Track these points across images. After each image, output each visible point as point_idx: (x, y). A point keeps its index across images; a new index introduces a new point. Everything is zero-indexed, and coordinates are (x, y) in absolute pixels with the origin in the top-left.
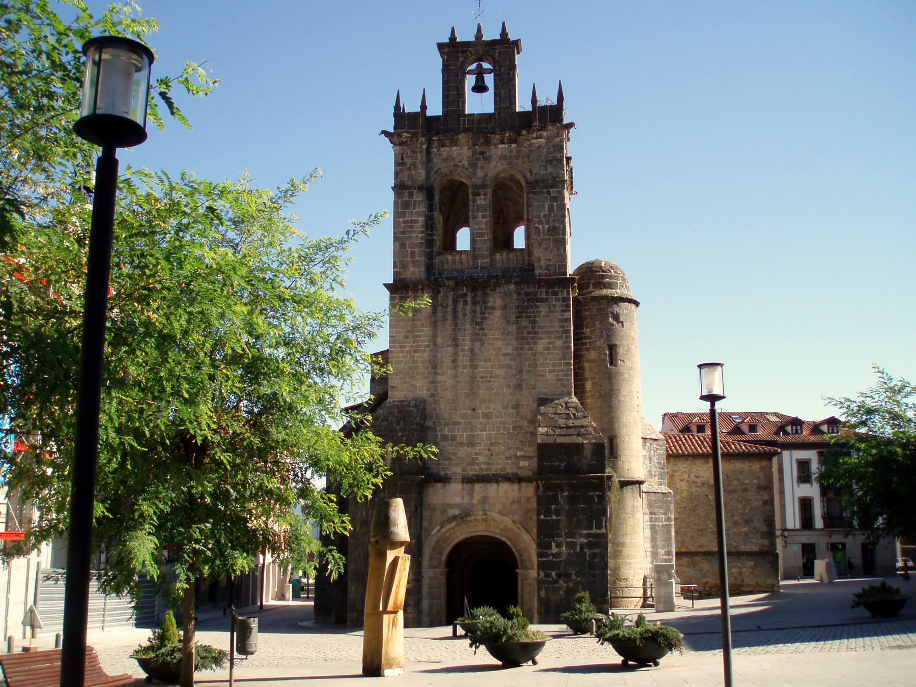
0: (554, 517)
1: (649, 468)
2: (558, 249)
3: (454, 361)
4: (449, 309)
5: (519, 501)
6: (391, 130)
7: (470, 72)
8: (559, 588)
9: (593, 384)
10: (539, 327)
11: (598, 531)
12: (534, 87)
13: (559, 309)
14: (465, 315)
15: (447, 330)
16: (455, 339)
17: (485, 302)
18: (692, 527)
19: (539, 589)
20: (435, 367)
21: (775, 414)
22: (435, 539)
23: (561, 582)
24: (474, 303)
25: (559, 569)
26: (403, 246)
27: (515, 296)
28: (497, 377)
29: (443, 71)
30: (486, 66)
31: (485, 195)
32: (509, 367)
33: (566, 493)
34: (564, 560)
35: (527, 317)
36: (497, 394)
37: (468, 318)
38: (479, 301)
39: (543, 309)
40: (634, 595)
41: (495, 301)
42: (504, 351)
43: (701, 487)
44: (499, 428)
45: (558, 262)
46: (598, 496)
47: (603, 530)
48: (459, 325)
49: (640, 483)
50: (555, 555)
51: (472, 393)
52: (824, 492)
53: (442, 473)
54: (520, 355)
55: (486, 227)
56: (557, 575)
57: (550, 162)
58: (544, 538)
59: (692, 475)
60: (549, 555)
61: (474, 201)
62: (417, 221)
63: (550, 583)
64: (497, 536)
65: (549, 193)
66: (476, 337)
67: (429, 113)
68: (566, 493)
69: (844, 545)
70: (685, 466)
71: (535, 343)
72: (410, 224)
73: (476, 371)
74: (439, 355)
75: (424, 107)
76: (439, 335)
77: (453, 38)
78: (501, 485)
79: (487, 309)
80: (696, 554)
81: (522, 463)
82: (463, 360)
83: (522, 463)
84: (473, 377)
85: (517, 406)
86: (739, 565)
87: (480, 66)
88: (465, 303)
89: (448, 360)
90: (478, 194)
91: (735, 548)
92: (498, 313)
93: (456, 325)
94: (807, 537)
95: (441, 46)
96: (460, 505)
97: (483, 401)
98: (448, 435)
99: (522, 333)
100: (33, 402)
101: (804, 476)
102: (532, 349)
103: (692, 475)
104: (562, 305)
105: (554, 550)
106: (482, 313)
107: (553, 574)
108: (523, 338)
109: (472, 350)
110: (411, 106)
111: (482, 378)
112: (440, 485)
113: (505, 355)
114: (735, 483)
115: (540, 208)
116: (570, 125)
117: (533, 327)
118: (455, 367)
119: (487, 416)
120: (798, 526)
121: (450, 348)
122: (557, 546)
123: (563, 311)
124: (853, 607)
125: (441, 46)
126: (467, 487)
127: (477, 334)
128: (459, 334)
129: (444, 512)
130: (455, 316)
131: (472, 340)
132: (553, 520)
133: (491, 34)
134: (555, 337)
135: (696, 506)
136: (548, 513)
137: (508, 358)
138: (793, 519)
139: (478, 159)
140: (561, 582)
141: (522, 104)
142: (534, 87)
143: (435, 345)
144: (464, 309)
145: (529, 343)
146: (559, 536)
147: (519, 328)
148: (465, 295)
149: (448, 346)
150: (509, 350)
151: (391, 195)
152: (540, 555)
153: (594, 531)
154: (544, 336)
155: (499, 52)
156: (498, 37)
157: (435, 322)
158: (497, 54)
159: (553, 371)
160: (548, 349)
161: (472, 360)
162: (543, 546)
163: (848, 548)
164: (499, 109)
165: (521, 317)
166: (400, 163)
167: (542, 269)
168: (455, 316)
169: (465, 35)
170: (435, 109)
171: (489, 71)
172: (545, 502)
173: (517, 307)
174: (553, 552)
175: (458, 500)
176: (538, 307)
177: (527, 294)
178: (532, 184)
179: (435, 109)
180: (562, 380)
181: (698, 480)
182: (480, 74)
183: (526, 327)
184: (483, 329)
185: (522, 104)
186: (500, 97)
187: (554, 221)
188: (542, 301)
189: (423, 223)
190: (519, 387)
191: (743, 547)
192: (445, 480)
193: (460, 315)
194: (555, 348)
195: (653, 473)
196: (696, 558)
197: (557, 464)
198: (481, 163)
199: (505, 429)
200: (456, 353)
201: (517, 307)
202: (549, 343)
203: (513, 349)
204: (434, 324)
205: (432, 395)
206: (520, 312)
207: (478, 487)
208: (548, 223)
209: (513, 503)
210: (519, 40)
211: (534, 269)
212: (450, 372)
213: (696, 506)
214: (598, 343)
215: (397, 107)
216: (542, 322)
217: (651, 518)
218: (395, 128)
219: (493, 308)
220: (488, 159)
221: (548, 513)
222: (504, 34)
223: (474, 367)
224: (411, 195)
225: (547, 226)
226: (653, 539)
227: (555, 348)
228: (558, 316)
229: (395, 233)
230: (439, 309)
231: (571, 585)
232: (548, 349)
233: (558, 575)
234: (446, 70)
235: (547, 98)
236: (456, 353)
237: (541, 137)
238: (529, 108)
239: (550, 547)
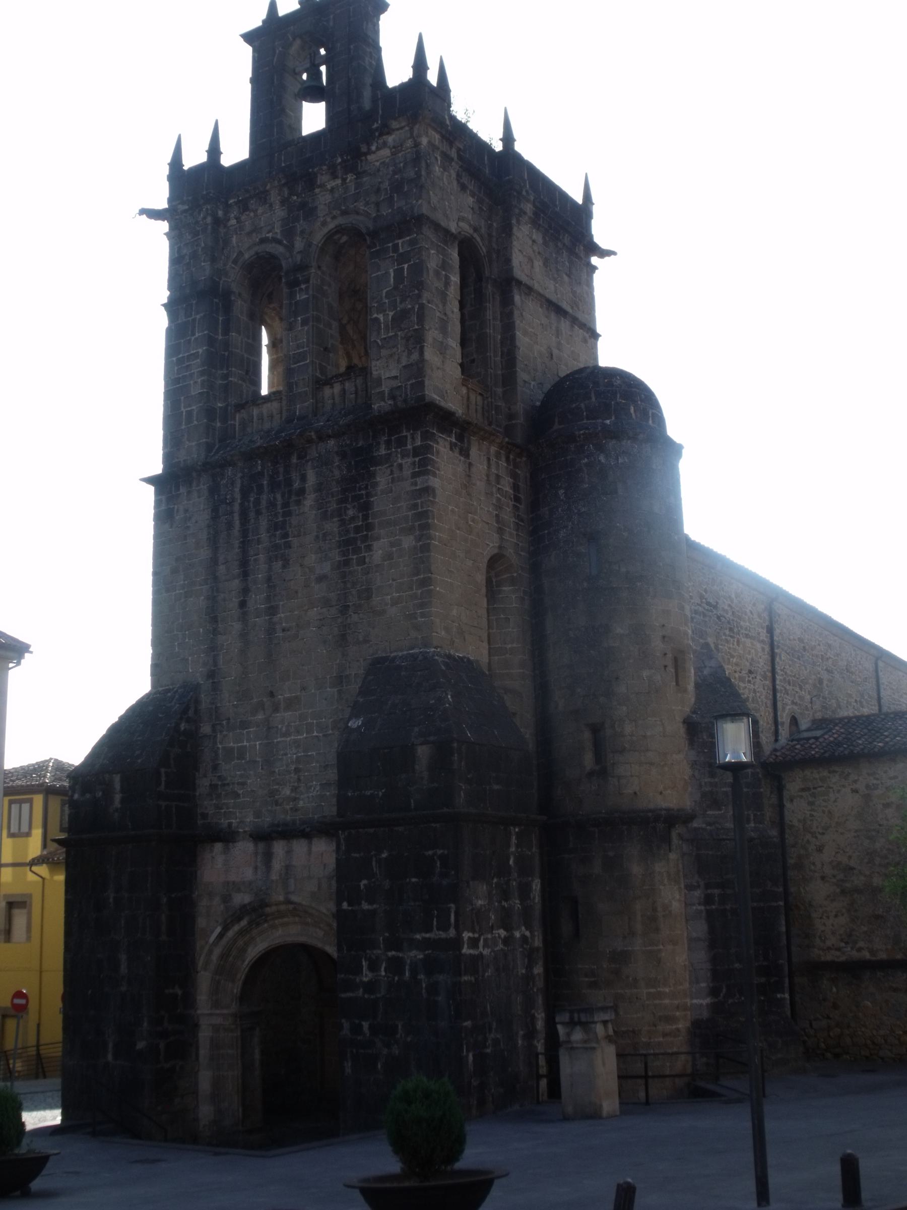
0: (365, 906)
2: (410, 354)
3: (243, 604)
4: (237, 507)
11: (443, 935)
13: (407, 472)
22: (217, 952)
41: (303, 478)
45: (408, 380)
47: (452, 933)
48: (250, 534)
53: (224, 822)
61: (292, 295)
64: (320, 945)
71: (369, 548)
75: (214, 150)
78: (315, 841)
82: (257, 600)
84: (271, 631)
98: (232, 749)
100: (825, 738)
102: (362, 561)
104: (414, 463)
105: (367, 976)
106: (286, 505)
107: (366, 1025)
111: (284, 630)
112: (218, 846)
117: (365, 517)
119: (291, 704)
126: (261, 846)
129: (226, 899)
143: (215, 578)
144: (257, 502)
147: (343, 522)
148: (261, 474)
153: (436, 934)
161: (268, 599)
167: (384, 400)
174: (365, 979)
175: (248, 874)
183: (353, 519)
192: (227, 837)
193: (252, 515)
197: (368, 793)
198: (301, 225)
200: (245, 591)
202: (392, 545)
207: (279, 848)
216: (380, 504)
219: (302, 492)
223: (272, 611)
225: (391, 314)
231: (396, 1051)
236: (245, 591)
237: (385, 144)
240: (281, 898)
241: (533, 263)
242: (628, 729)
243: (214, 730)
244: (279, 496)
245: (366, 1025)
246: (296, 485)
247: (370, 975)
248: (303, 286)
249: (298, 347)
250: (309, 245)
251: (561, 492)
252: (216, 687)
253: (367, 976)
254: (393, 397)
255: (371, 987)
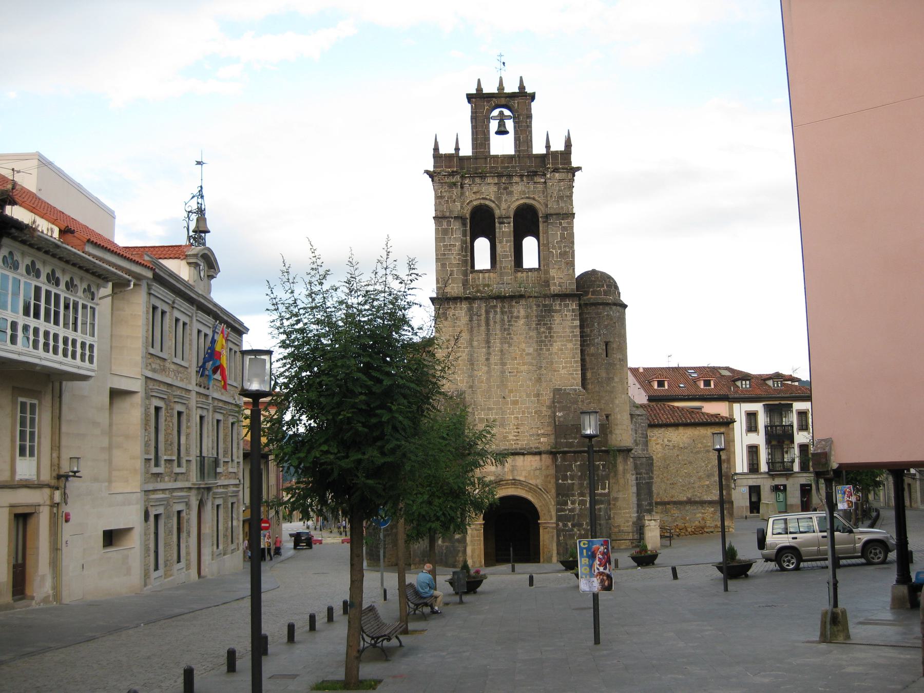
1: (635, 438)
2: (568, 270)
3: (488, 359)
5: (540, 469)
6: (431, 169)
7: (494, 118)
8: (574, 535)
9: (592, 373)
10: (554, 332)
11: (603, 491)
12: (548, 135)
14: (495, 322)
15: (482, 335)
16: (488, 342)
17: (511, 312)
18: (665, 481)
19: (558, 536)
20: (472, 364)
21: (727, 369)
23: (575, 530)
24: (503, 313)
25: (574, 520)
26: (443, 265)
27: (535, 308)
28: (522, 372)
29: (472, 118)
30: (507, 112)
31: (509, 223)
32: (531, 364)
33: (579, 463)
34: (577, 514)
35: (545, 324)
36: (522, 386)
37: (498, 327)
38: (506, 311)
39: (557, 318)
40: (621, 538)
41: (519, 312)
42: (527, 351)
43: (672, 449)
44: (523, 412)
46: (602, 465)
47: (607, 491)
48: (491, 331)
49: (630, 450)
50: (570, 510)
51: (503, 384)
52: (768, 441)
54: (539, 355)
55: (510, 250)
56: (572, 524)
57: (561, 198)
58: (562, 497)
59: (666, 440)
60: (565, 510)
61: (500, 228)
62: (454, 245)
63: (567, 531)
65: (561, 224)
66: (504, 341)
67: (461, 154)
68: (579, 463)
69: (785, 486)
70: (660, 432)
71: (551, 345)
72: (448, 247)
73: (505, 367)
74: (475, 355)
76: (475, 339)
77: (479, 89)
79: (513, 318)
80: (668, 503)
81: (542, 440)
83: (542, 440)
84: (503, 372)
85: (538, 395)
86: (703, 511)
87: (501, 113)
88: (496, 312)
89: (482, 358)
90: (503, 223)
91: (699, 497)
92: (522, 322)
93: (488, 330)
94: (753, 480)
95: (470, 97)
96: (494, 472)
97: (511, 391)
99: (541, 337)
101: (752, 427)
103: (666, 440)
105: (570, 506)
106: (509, 321)
107: (570, 524)
108: (542, 341)
109: (502, 351)
110: (447, 148)
113: (528, 354)
114: (700, 445)
115: (554, 233)
116: (579, 169)
117: (550, 333)
118: (488, 366)
119: (515, 403)
120: (746, 470)
121: (484, 350)
122: (572, 504)
123: (572, 320)
124: (380, 681)
125: (470, 97)
127: (506, 338)
128: (491, 338)
130: (487, 324)
131: (502, 343)
132: (569, 483)
133: (511, 87)
134: (567, 340)
135: (669, 465)
136: (565, 478)
137: (530, 357)
138: (741, 464)
139: (501, 194)
140: (575, 530)
141: (538, 148)
142: (548, 135)
143: (472, 346)
144: (494, 317)
145: (545, 345)
146: (573, 495)
147: (539, 333)
148: (495, 306)
149: (482, 348)
150: (531, 350)
151: (431, 226)
152: (558, 510)
154: (558, 340)
155: (518, 103)
156: (517, 91)
157: (472, 328)
158: (516, 105)
159: (566, 367)
160: (562, 350)
161: (501, 359)
162: (561, 504)
163: (788, 488)
164: (519, 151)
165: (540, 324)
166: (438, 197)
168: (487, 324)
169: (490, 88)
170: (466, 150)
171: (509, 117)
172: (560, 472)
173: (537, 316)
176: (553, 316)
177: (545, 306)
178: (547, 216)
179: (466, 150)
180: (572, 374)
181: (670, 444)
182: (502, 119)
184: (510, 334)
185: (538, 148)
186: (520, 140)
187: (565, 247)
188: (556, 311)
189: (460, 247)
190: (539, 380)
191: (705, 497)
193: (492, 323)
194: (567, 349)
195: (638, 441)
196: (668, 506)
197: (571, 441)
198: (504, 197)
199: (529, 413)
200: (489, 354)
201: (537, 316)
202: (562, 345)
203: (534, 350)
204: (471, 331)
205: (471, 387)
206: (539, 320)
208: (560, 248)
209: (536, 469)
210: (534, 93)
211: (549, 286)
212: (485, 368)
213: (669, 465)
214: (596, 341)
215: (436, 149)
216: (556, 328)
217: (637, 478)
218: (435, 167)
219: (518, 317)
220: (510, 193)
221: (565, 478)
222: (522, 87)
223: (503, 364)
224: (449, 224)
225: (559, 251)
226: (638, 494)
227: (567, 349)
228: (569, 323)
229: (437, 255)
230: (475, 318)
232: (562, 350)
233: (573, 526)
234: (475, 118)
235: (558, 146)
238: (544, 151)
239: (566, 504)
240: (511, 478)
241: (551, 215)
242: (619, 416)
243: (473, 410)
244: (506, 318)
245: (570, 524)
246: (515, 314)
247: (572, 506)
248: (506, 225)
249: (504, 251)
250: (509, 207)
251: (596, 324)
252: (474, 392)
253: (570, 506)
254: (560, 286)
255: (572, 510)
